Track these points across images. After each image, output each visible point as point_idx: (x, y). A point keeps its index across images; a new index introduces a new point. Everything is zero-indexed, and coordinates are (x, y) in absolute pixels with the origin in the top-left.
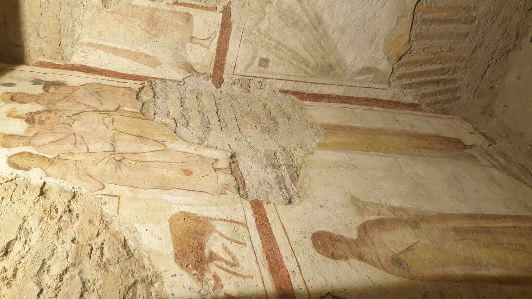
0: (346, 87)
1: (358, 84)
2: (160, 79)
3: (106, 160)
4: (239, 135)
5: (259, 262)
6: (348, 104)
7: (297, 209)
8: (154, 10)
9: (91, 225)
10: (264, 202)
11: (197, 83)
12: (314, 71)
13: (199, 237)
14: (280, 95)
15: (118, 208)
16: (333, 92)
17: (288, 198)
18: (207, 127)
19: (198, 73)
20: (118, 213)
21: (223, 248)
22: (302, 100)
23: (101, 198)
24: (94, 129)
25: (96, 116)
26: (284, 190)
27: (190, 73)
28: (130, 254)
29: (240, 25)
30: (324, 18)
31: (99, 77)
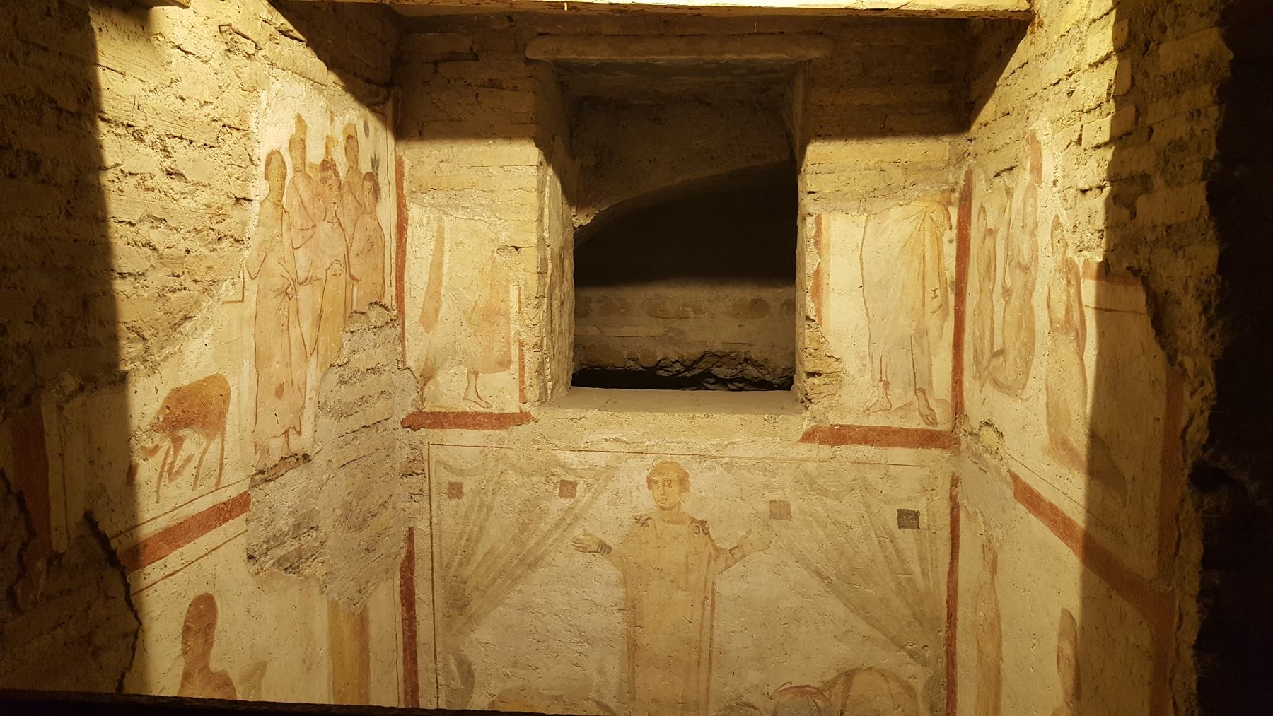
0: (433, 645)
1: (440, 665)
2: (403, 332)
3: (286, 275)
4: (335, 465)
5: (176, 511)
6: (404, 656)
7: (242, 569)
8: (507, 315)
9: (206, 269)
10: (248, 513)
11: (406, 390)
12: (455, 578)
13: (201, 420)
14: (405, 530)
15: (229, 302)
16: (422, 623)
17: (255, 554)
18: (343, 413)
19: (422, 389)
20: (223, 303)
21: (189, 457)
22: (401, 571)
23: (239, 277)
24: (324, 252)
25: (341, 249)
26: (265, 546)
27: (421, 376)
28: (175, 327)
29: (506, 442)
30: (539, 570)
31: (394, 244)
